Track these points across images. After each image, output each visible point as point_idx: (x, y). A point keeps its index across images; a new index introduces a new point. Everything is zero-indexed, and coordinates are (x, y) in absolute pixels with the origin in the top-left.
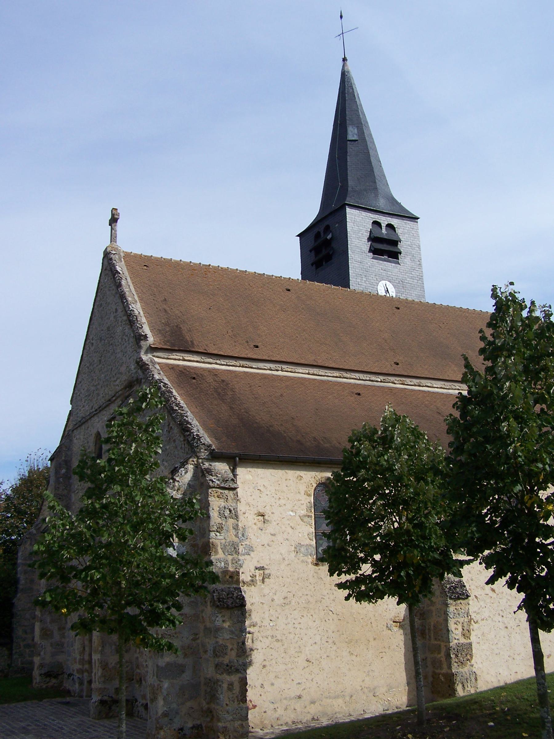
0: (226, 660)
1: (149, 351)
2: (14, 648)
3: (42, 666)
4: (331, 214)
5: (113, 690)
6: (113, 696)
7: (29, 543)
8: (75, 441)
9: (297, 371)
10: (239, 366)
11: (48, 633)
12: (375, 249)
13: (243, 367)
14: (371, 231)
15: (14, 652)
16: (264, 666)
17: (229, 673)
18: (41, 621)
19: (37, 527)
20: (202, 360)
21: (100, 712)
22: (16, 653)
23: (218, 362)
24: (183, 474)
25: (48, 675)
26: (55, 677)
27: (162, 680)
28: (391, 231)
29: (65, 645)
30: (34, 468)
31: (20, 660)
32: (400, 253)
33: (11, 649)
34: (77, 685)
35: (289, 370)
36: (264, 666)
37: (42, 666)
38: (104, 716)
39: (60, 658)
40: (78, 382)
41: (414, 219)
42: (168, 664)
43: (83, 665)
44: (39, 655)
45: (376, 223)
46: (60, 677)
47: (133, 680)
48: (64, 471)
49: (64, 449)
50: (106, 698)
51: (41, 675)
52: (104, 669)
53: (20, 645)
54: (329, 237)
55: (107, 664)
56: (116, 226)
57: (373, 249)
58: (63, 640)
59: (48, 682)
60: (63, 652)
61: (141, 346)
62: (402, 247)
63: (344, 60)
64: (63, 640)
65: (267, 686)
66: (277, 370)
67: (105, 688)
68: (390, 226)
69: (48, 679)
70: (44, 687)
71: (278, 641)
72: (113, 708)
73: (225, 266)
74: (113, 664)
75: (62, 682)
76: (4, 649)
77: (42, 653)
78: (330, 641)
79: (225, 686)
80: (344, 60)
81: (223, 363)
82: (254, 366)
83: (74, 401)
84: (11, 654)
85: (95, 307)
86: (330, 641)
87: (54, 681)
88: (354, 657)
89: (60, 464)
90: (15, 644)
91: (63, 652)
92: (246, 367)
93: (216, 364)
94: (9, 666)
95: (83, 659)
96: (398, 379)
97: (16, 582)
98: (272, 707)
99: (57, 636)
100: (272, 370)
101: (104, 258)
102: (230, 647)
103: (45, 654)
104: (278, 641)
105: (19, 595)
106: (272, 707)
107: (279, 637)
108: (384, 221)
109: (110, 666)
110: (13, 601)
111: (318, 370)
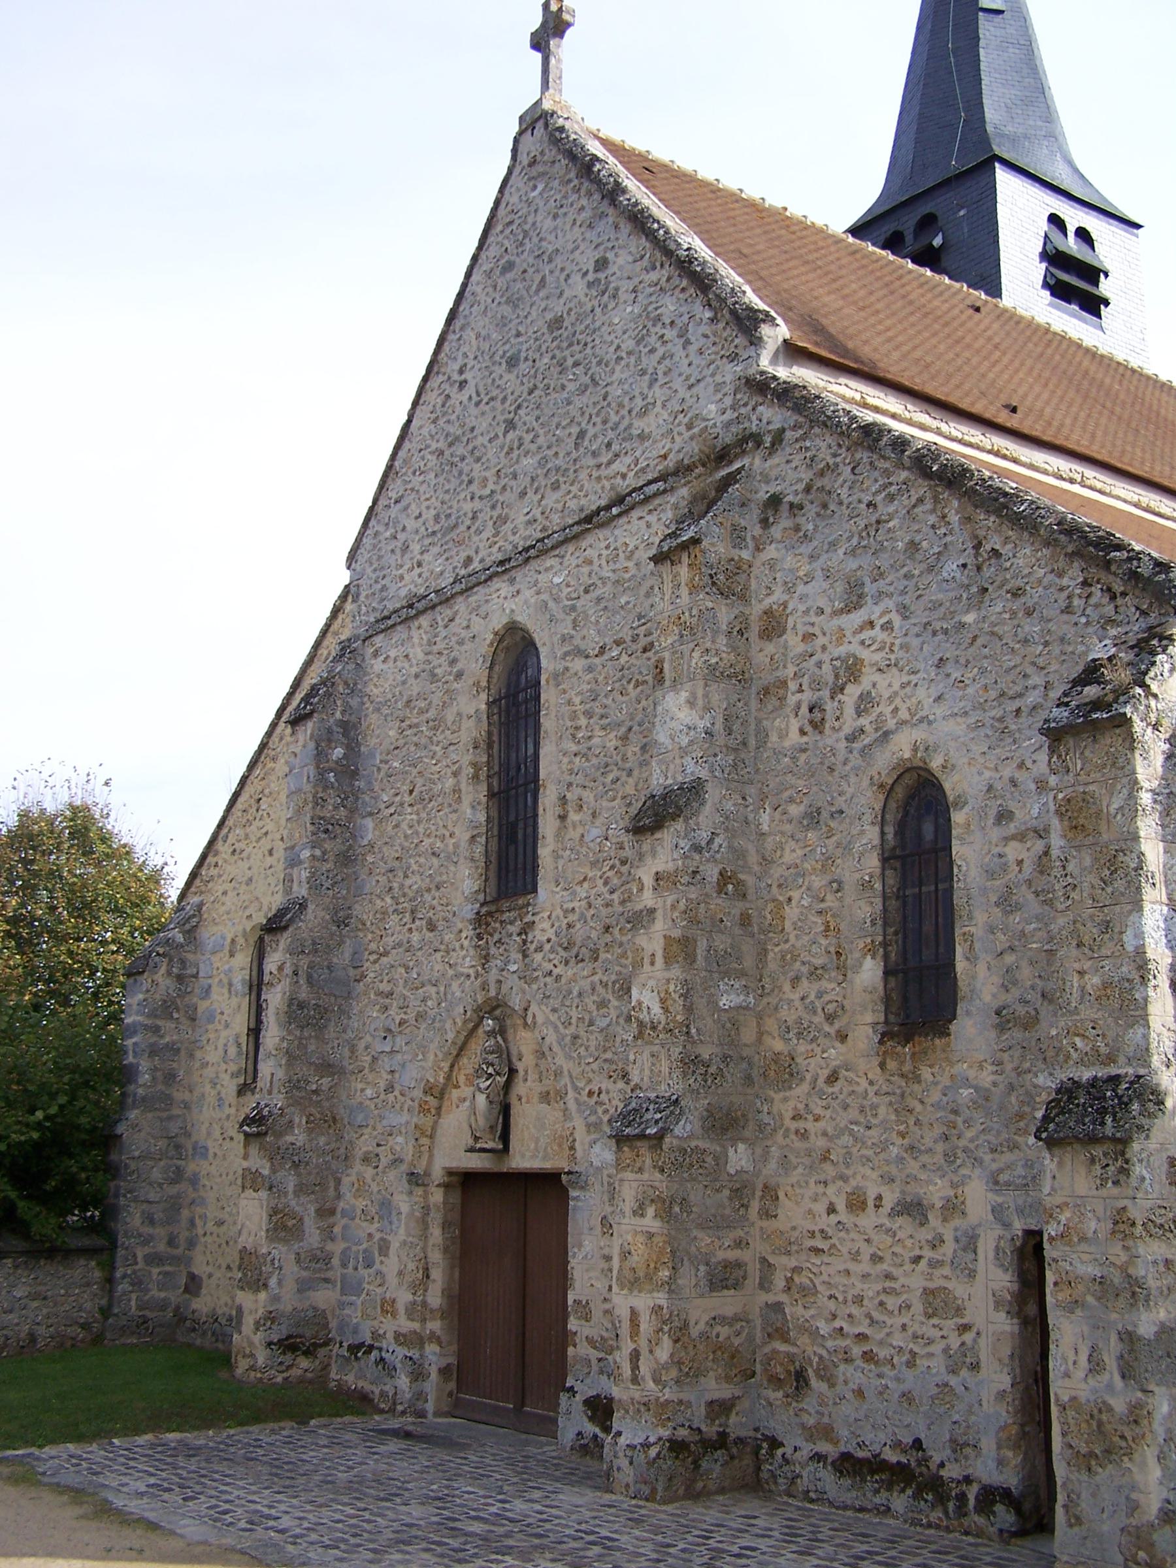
1: (781, 356)
2: (118, 1264)
3: (273, 1320)
4: (945, 184)
5: (703, 1409)
6: (704, 1428)
7: (163, 970)
8: (377, 665)
9: (1116, 492)
10: (989, 452)
11: (290, 1223)
12: (1058, 281)
13: (997, 454)
14: (1046, 236)
15: (118, 1275)
18: (270, 1188)
19: (187, 927)
20: (908, 415)
21: (670, 1479)
22: (124, 1276)
23: (944, 427)
24: (1166, 674)
25: (289, 1345)
26: (306, 1353)
27: (1151, 1387)
28: (1085, 248)
29: (336, 1261)
31: (134, 1296)
32: (1107, 304)
33: (110, 1267)
34: (403, 1381)
35: (1099, 485)
37: (271, 1318)
38: (681, 1492)
39: (323, 1297)
40: (382, 502)
41: (1138, 226)
43: (424, 1321)
44: (265, 1285)
45: (1055, 221)
46: (322, 1352)
47: (753, 1374)
48: (339, 752)
49: (341, 689)
50: (683, 1433)
51: (269, 1344)
52: (676, 1341)
53: (135, 1256)
54: (937, 241)
55: (686, 1325)
56: (559, 46)
57: (1052, 282)
58: (330, 1246)
59: (289, 1367)
60: (327, 1280)
61: (760, 339)
62: (1106, 287)
64: (330, 1246)
66: (1072, 481)
67: (681, 1402)
68: (1083, 235)
69: (288, 1358)
70: (279, 1379)
72: (704, 1464)
73: (819, 222)
74: (702, 1326)
75: (326, 1367)
76: (93, 1263)
77: (273, 1282)
81: (955, 433)
82: (1023, 459)
83: (363, 555)
84: (110, 1281)
85: (475, 278)
87: (304, 1363)
89: (330, 731)
90: (121, 1252)
91: (327, 1280)
92: (1004, 457)
93: (939, 432)
94: (106, 1312)
95: (424, 1303)
97: (127, 1075)
99: (313, 1235)
100: (1061, 478)
101: (521, 133)
103: (280, 1283)
105: (133, 1114)
108: (1074, 217)
109: (695, 1332)
110: (119, 1131)
111: (1158, 498)
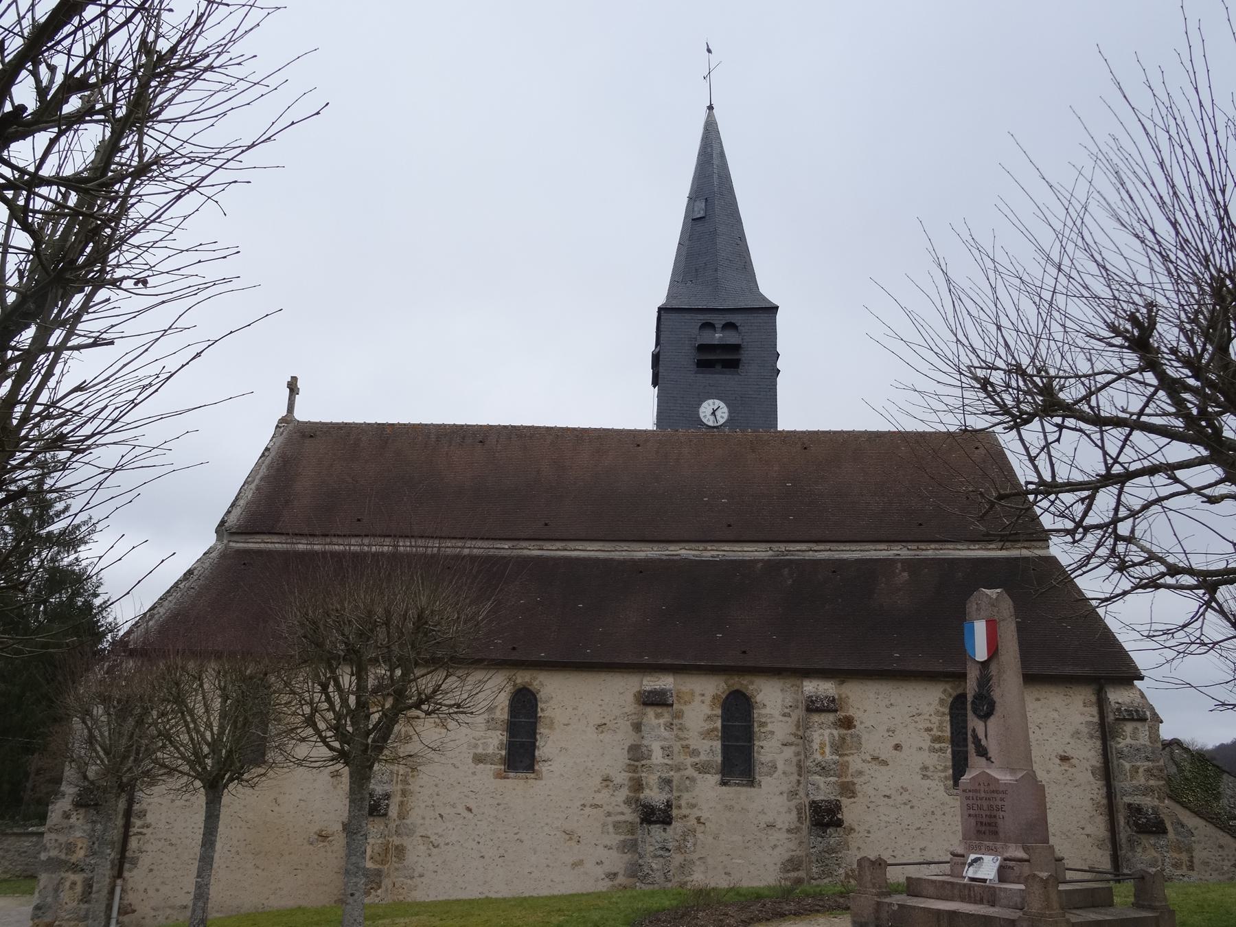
0: (74, 859)
16: (151, 870)
17: (74, 872)
30: (1180, 769)
36: (151, 870)
42: (49, 858)
63: (711, 108)
65: (151, 892)
71: (171, 844)
78: (233, 850)
79: (68, 884)
80: (711, 108)
86: (233, 850)
88: (259, 871)
96: (533, 543)
98: (153, 913)
102: (80, 845)
104: (171, 844)
106: (153, 913)
107: (174, 841)
